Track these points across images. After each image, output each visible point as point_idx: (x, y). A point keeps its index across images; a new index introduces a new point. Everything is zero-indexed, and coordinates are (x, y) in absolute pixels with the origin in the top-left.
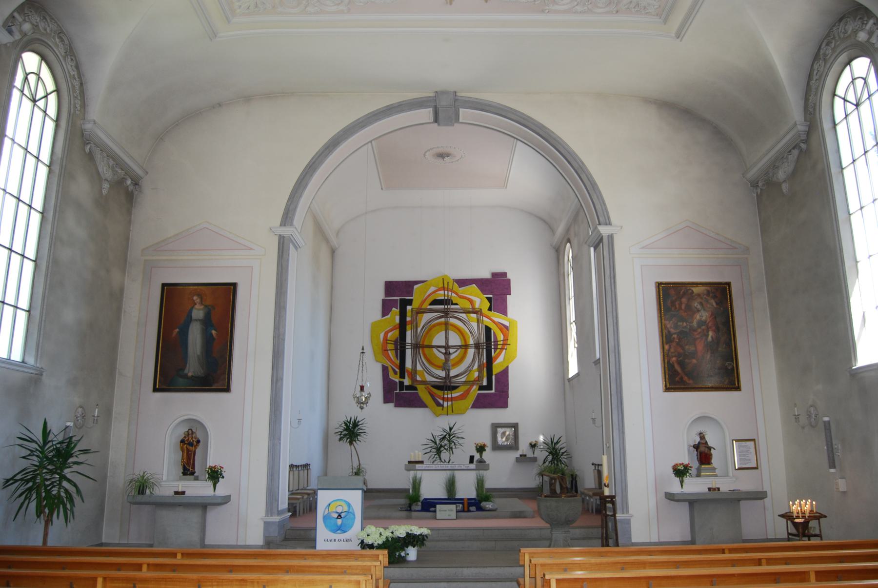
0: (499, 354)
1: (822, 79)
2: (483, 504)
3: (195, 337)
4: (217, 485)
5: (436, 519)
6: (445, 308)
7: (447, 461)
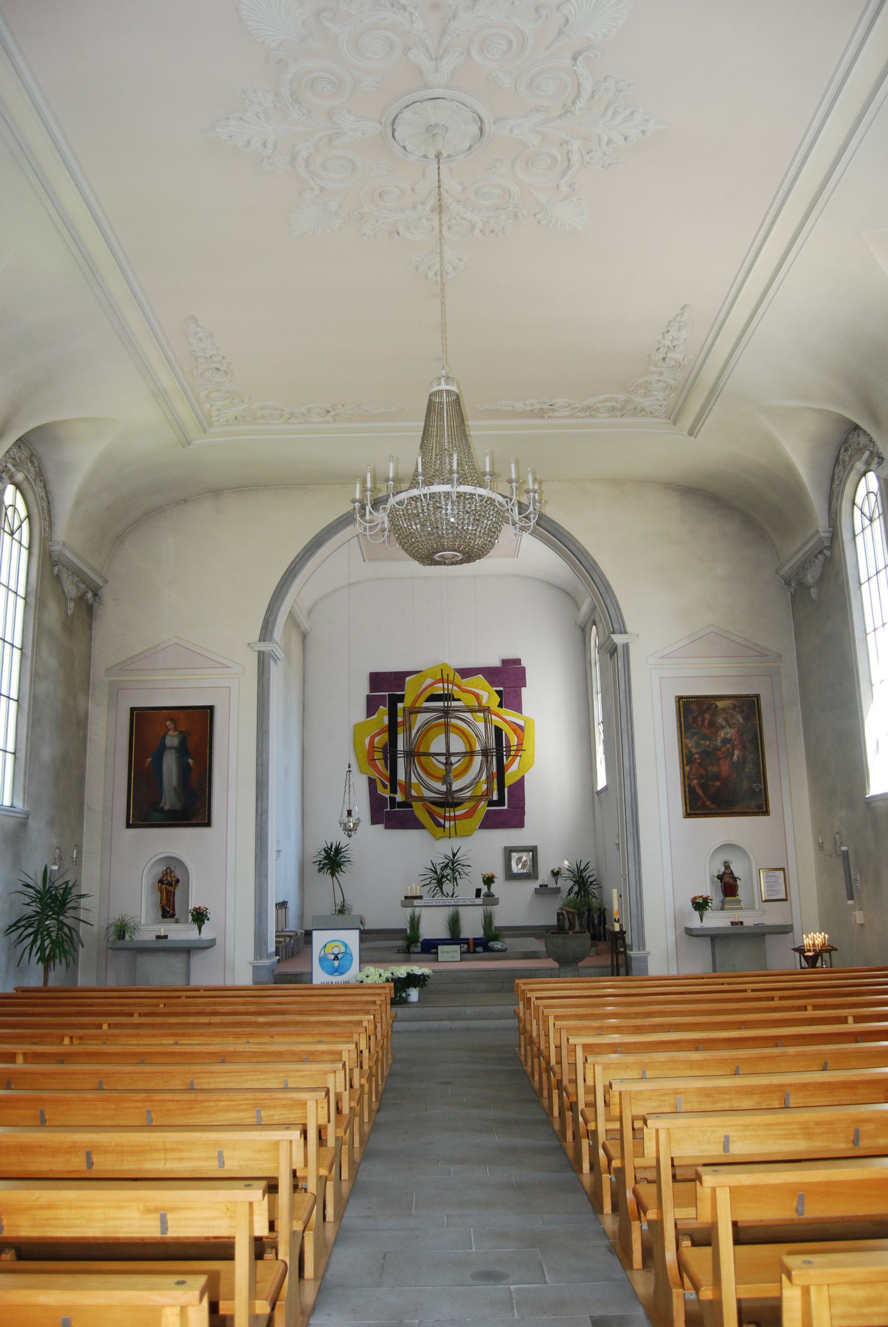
0: (512, 762)
1: (842, 484)
2: (491, 944)
3: (170, 765)
4: (203, 928)
5: (438, 961)
6: (444, 706)
7: (451, 894)
